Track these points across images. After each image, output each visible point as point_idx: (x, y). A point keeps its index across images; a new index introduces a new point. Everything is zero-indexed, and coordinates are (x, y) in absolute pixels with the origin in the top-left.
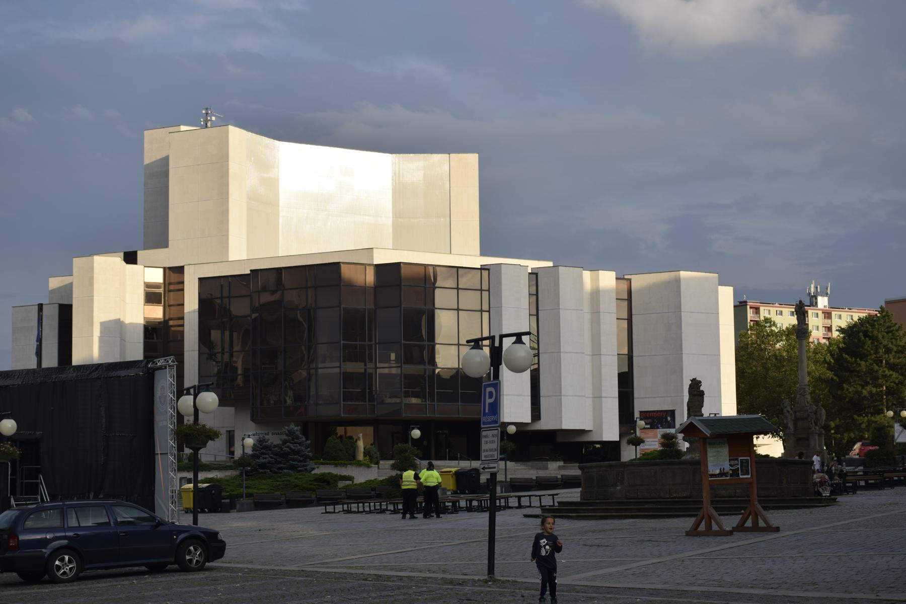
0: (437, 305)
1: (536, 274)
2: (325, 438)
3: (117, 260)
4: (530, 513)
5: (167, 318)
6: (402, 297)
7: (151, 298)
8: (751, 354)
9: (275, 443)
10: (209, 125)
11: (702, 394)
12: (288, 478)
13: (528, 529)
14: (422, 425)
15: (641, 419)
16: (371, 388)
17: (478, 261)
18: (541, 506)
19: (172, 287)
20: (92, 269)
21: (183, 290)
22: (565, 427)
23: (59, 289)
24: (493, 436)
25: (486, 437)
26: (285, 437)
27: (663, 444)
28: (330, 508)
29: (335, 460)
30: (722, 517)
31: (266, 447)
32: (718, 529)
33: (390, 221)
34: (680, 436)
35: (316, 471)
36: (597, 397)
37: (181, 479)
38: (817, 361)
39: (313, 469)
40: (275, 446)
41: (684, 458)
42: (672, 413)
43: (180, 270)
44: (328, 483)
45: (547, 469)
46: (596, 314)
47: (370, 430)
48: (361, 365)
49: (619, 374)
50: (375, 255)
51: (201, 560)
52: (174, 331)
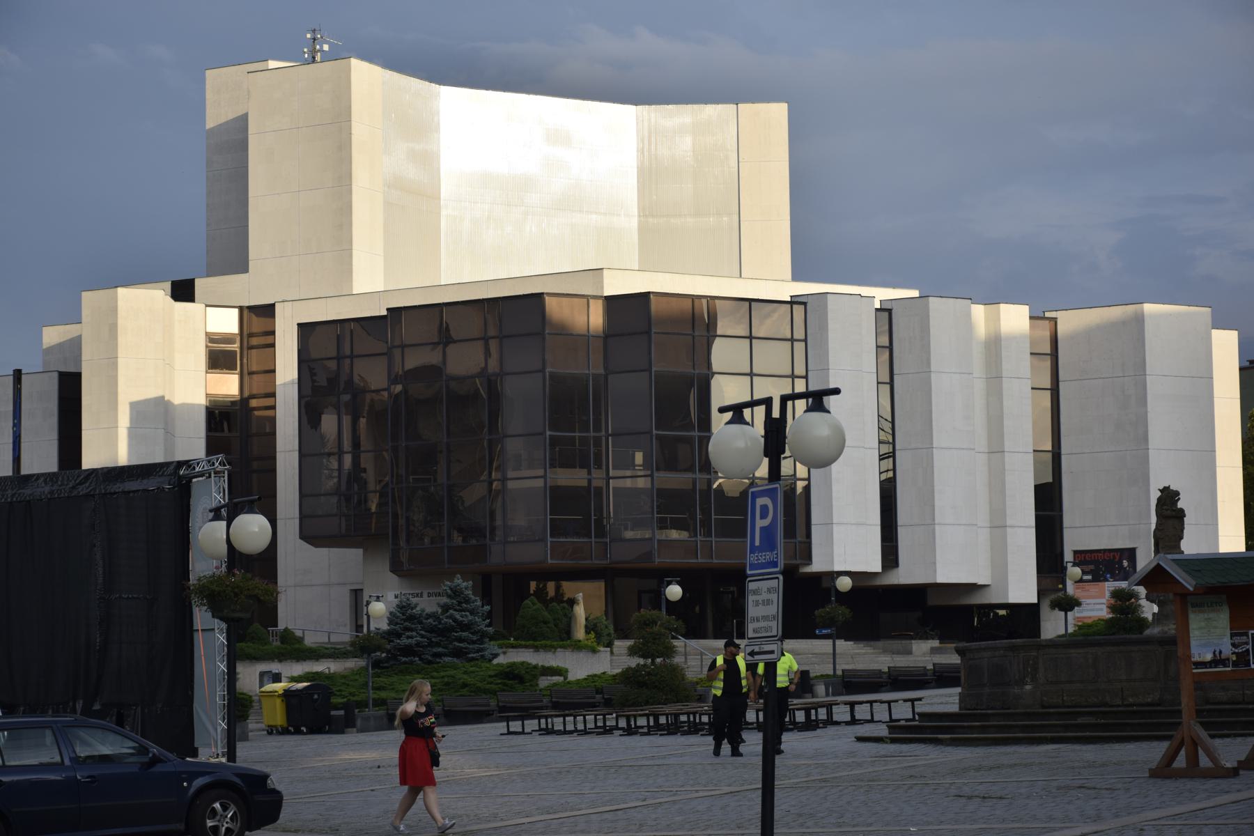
0: (715, 368)
1: (890, 311)
2: (520, 601)
3: (159, 295)
4: (867, 735)
5: (246, 394)
6: (651, 354)
7: (218, 360)
9: (429, 610)
10: (318, 58)
11: (1181, 515)
12: (452, 672)
13: (860, 765)
14: (684, 576)
15: (1075, 564)
16: (599, 509)
17: (786, 290)
18: (891, 720)
19: (255, 341)
20: (114, 310)
21: (273, 345)
22: (941, 578)
23: (60, 346)
24: (769, 591)
25: (755, 592)
26: (445, 600)
27: (1112, 608)
28: (516, 726)
29: (535, 640)
30: (1217, 742)
31: (411, 618)
32: (1210, 765)
33: (634, 223)
34: (1142, 590)
35: (501, 660)
36: (998, 526)
37: (262, 674)
39: (496, 656)
40: (429, 616)
41: (1147, 632)
42: (1131, 553)
43: (267, 311)
44: (520, 679)
45: (910, 652)
46: (994, 379)
47: (598, 587)
48: (583, 473)
49: (1036, 487)
50: (606, 281)
51: (236, 827)
52: (259, 417)
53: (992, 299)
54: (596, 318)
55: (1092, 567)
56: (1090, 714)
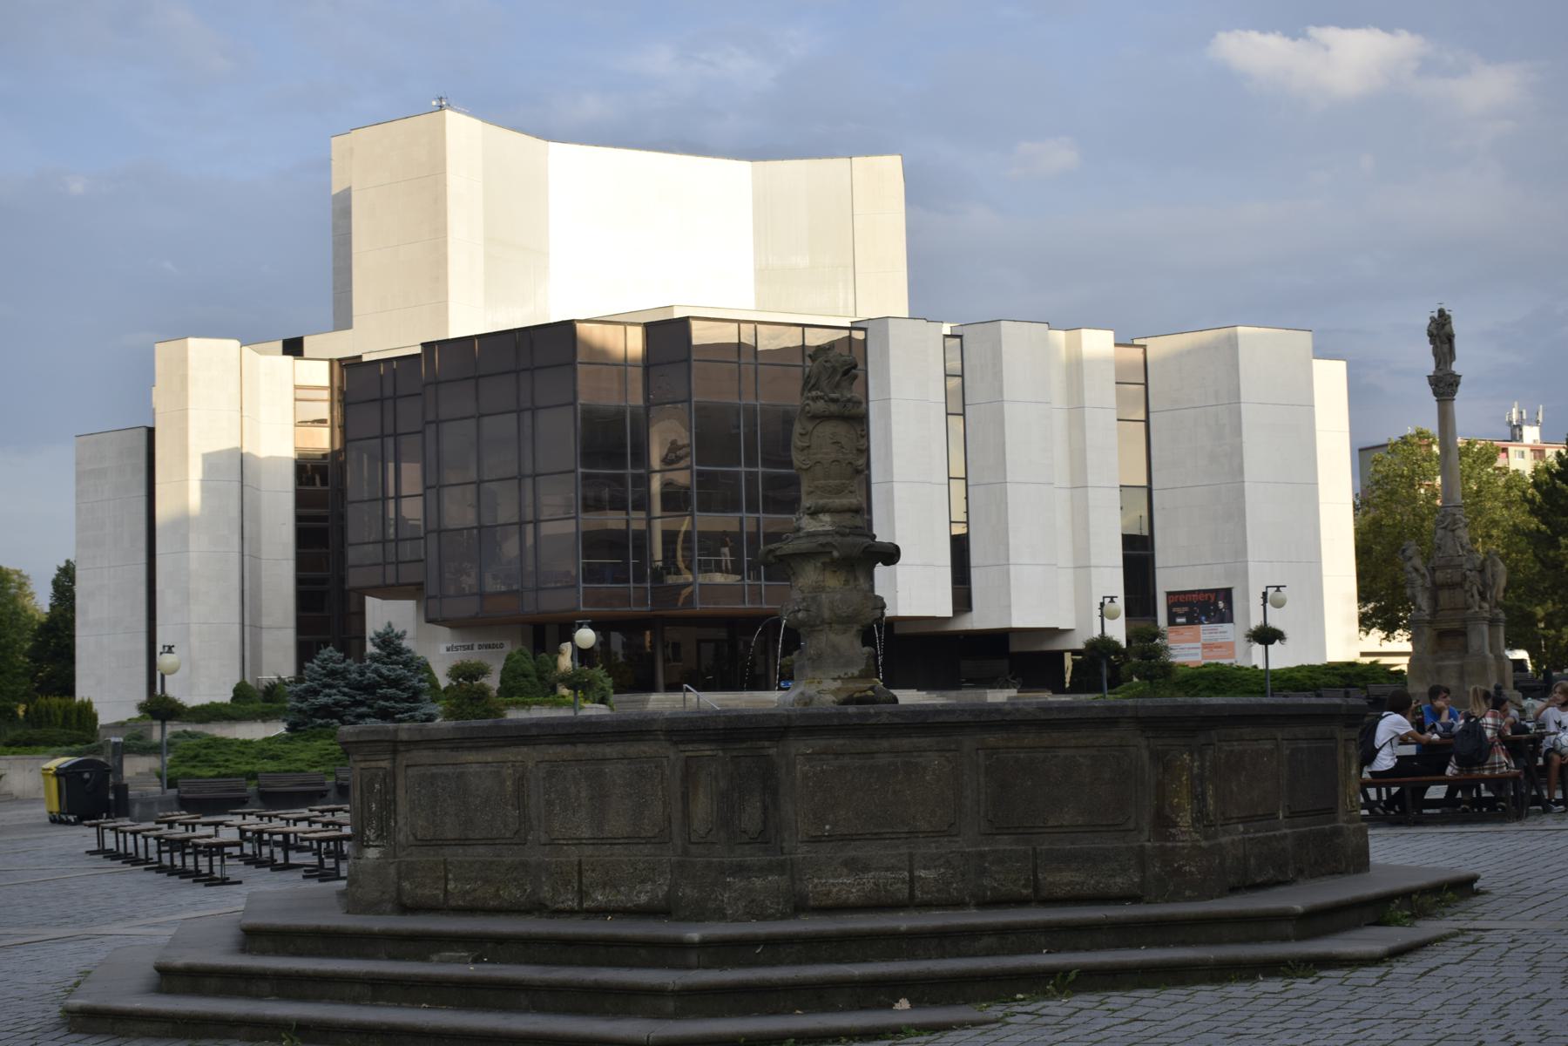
8: (1393, 492)
22: (1017, 623)
38: (1512, 502)
46: (1076, 409)
48: (621, 515)
53: (1072, 326)
54: (634, 343)
55: (1186, 609)
56: (478, 945)
